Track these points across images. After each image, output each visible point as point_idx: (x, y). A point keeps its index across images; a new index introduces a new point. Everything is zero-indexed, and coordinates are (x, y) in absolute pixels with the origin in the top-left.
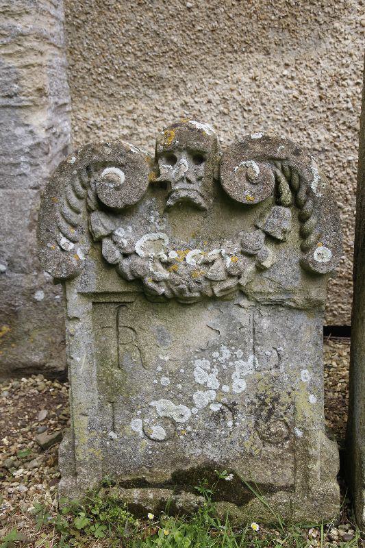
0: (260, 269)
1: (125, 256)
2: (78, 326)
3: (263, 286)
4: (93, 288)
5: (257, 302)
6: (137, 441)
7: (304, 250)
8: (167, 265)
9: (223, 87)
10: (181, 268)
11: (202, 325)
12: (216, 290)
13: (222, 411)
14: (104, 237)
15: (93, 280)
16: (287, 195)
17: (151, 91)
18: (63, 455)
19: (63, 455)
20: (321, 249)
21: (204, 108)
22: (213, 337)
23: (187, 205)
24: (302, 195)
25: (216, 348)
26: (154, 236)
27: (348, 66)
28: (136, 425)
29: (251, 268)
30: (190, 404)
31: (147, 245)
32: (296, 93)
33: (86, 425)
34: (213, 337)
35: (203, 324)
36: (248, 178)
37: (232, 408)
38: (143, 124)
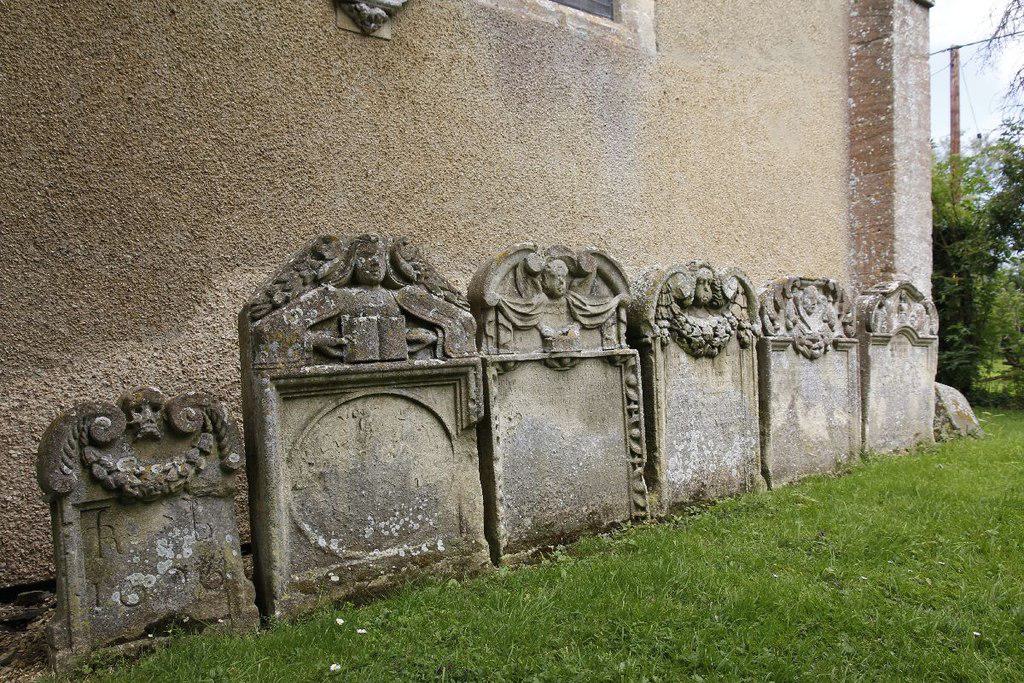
0: (198, 471)
1: (109, 473)
2: (71, 528)
3: (200, 484)
4: (84, 499)
5: (195, 495)
6: (119, 607)
7: (222, 457)
8: (139, 476)
9: (105, 365)
10: (149, 477)
11: (159, 516)
12: (173, 487)
13: (177, 573)
14: (95, 462)
15: (83, 494)
16: (210, 427)
17: (40, 370)
18: (59, 633)
19: (59, 633)
20: (233, 455)
21: (90, 382)
22: (168, 522)
23: (151, 437)
24: (219, 425)
25: (170, 529)
26: (127, 459)
27: (201, 350)
28: (116, 597)
29: (193, 471)
30: (155, 572)
31: (122, 465)
32: (165, 369)
33: (79, 602)
34: (168, 522)
35: (161, 514)
36: (188, 417)
37: (184, 570)
38: (32, 396)
